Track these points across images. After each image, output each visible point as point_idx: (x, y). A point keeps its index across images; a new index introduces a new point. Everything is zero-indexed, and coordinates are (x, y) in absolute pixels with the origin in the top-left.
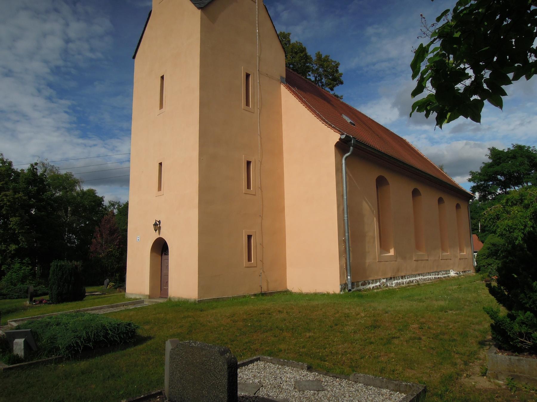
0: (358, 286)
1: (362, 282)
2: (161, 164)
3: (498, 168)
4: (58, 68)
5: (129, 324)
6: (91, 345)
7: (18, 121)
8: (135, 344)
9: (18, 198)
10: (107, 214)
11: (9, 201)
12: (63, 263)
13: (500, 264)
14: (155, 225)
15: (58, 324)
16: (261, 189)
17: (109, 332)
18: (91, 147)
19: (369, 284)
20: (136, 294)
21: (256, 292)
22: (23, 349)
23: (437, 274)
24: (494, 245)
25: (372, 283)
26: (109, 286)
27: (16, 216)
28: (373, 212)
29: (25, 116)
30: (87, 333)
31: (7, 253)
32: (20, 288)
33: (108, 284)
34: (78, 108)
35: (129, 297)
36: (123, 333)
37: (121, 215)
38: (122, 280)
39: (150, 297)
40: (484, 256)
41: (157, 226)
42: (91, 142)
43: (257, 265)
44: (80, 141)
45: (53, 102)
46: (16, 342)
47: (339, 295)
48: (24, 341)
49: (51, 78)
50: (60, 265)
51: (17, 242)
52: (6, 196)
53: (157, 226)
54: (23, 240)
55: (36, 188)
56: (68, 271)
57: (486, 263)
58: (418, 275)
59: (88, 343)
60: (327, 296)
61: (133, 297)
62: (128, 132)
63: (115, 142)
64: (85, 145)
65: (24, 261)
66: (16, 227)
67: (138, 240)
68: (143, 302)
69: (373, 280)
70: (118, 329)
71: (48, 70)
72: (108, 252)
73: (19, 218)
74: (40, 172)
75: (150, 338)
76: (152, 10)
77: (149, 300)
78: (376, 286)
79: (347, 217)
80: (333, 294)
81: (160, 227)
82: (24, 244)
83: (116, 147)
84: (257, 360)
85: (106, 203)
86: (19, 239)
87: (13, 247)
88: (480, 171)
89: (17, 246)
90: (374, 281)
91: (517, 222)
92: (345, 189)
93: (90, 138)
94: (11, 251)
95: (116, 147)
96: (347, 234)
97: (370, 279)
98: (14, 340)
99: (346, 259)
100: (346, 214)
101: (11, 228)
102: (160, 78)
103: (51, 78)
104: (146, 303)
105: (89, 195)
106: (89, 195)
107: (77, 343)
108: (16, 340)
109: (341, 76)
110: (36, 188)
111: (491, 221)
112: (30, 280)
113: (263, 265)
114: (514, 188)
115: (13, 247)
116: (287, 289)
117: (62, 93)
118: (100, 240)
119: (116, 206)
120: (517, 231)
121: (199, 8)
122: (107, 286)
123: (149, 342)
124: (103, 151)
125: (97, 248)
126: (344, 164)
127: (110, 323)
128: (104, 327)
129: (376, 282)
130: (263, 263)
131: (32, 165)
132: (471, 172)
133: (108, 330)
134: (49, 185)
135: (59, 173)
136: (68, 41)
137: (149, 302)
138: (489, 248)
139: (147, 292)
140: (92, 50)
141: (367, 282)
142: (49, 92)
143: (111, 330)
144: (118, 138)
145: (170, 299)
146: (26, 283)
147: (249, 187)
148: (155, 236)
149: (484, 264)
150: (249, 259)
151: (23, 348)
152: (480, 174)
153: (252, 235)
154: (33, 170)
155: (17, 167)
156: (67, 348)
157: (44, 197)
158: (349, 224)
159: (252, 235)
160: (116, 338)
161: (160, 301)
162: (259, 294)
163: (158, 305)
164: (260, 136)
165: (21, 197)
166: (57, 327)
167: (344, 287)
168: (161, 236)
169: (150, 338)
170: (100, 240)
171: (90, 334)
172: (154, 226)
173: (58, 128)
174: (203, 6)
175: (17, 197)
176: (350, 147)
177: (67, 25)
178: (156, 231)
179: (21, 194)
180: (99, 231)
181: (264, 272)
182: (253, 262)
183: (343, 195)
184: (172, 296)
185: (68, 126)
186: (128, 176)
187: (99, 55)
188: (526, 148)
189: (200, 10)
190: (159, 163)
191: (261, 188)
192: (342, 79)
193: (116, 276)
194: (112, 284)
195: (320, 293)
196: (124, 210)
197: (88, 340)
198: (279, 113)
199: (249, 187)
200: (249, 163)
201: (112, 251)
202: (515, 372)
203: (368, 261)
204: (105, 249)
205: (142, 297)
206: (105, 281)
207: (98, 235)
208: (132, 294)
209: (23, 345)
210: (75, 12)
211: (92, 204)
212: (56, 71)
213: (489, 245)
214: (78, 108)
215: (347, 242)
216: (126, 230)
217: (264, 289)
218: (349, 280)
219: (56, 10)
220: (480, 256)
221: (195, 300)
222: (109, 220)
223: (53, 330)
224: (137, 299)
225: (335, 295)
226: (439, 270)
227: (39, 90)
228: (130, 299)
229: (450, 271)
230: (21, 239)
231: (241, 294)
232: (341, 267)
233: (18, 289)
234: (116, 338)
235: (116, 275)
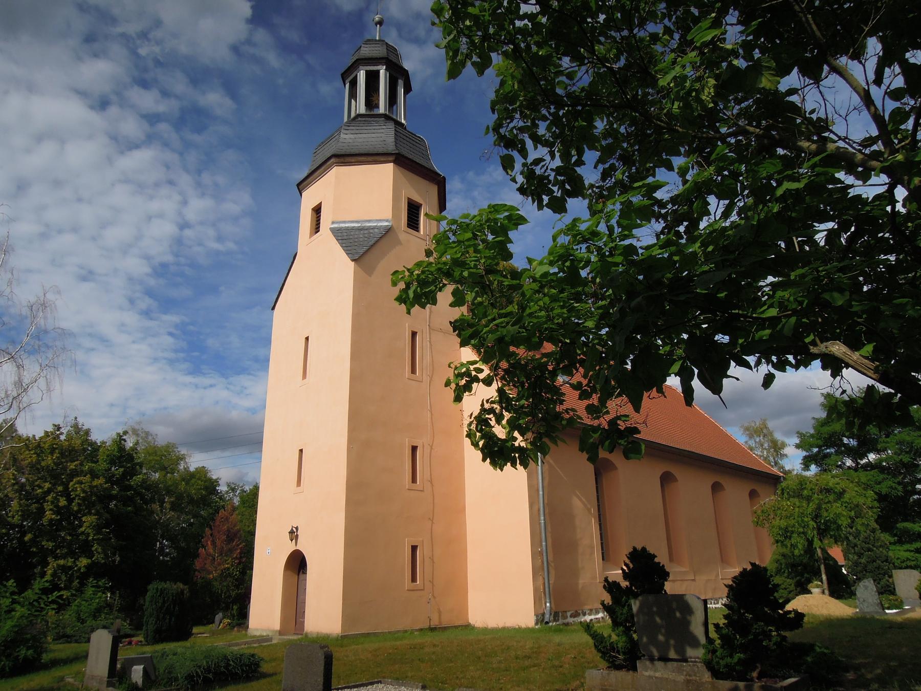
0: (566, 618)
1: (572, 612)
2: (301, 451)
4: (164, 266)
5: (253, 656)
6: (210, 676)
7: (93, 349)
8: (258, 678)
9: (96, 486)
10: (223, 507)
11: (84, 491)
12: (165, 586)
13: (793, 585)
14: (292, 532)
15: (175, 654)
16: (431, 483)
17: (231, 663)
18: (205, 388)
19: (584, 614)
20: (263, 630)
21: (421, 626)
23: (713, 601)
25: (590, 614)
26: (221, 624)
27: (90, 513)
28: (589, 510)
29: (104, 341)
30: (207, 662)
31: (73, 571)
32: (92, 626)
33: (221, 622)
34: (191, 328)
35: (252, 635)
36: (246, 666)
37: (244, 507)
38: (243, 615)
39: (281, 633)
41: (294, 534)
42: (207, 381)
44: (189, 379)
45: (151, 319)
48: (144, 668)
49: (152, 282)
50: (161, 589)
51: (90, 555)
52: (81, 483)
53: (294, 534)
54: (100, 550)
55: (122, 470)
56: (171, 597)
59: (209, 673)
60: (519, 631)
61: (258, 633)
62: (264, 363)
63: (244, 380)
64: (197, 386)
65: (100, 583)
66: (90, 531)
69: (591, 610)
70: (241, 660)
71: (148, 270)
72: (222, 571)
73: (96, 517)
74: (129, 443)
75: (275, 674)
77: (280, 637)
78: (596, 618)
79: (545, 520)
80: (525, 629)
81: (297, 536)
82: (99, 557)
83: (245, 388)
84: (378, 682)
85: (223, 488)
86: (93, 549)
87: (84, 562)
88: (812, 431)
89: (89, 561)
90: (594, 610)
91: (793, 521)
92: (540, 481)
93: (204, 374)
94: (80, 569)
95: (245, 388)
96: (544, 543)
97: (586, 608)
98: (132, 667)
99: (544, 579)
101: (84, 532)
103: (152, 282)
104: (274, 642)
105: (199, 479)
106: (199, 479)
107: (197, 672)
108: (135, 667)
110: (122, 470)
112: (106, 614)
113: (433, 588)
115: (84, 562)
117: (167, 304)
118: (211, 551)
119: (238, 492)
120: (795, 535)
122: (219, 625)
123: (274, 677)
124: (224, 394)
125: (205, 564)
127: (232, 653)
128: (225, 657)
129: (596, 612)
130: (433, 585)
131: (118, 434)
132: (798, 433)
133: (229, 660)
134: (141, 465)
135: (156, 443)
136: (184, 225)
137: (280, 639)
138: (778, 560)
139: (277, 626)
140: (220, 239)
141: (581, 612)
142: (145, 303)
143: (233, 661)
144: (249, 374)
145: (306, 635)
146: (100, 619)
147: (414, 480)
148: (290, 547)
150: (414, 579)
152: (812, 436)
154: (120, 442)
155: (97, 437)
156: (186, 678)
157: (132, 483)
158: (549, 528)
160: (238, 670)
162: (426, 629)
163: (291, 644)
164: (431, 412)
165: (101, 485)
166: (175, 657)
167: (540, 619)
168: (299, 547)
169: (275, 674)
170: (211, 551)
171: (210, 663)
173: (156, 360)
175: (95, 484)
177: (185, 203)
178: (292, 540)
179: (101, 481)
180: (211, 535)
181: (434, 597)
183: (538, 490)
185: (172, 355)
186: (261, 433)
187: (231, 245)
191: (431, 482)
193: (233, 609)
194: (227, 621)
196: (251, 499)
197: (208, 670)
199: (414, 480)
200: (414, 449)
201: (228, 569)
202: (605, 686)
203: (581, 582)
204: (219, 564)
205: (270, 634)
206: (217, 616)
207: (209, 543)
208: (257, 630)
209: (142, 672)
210: (199, 185)
211: (202, 493)
212: (161, 270)
214: (191, 328)
215: (544, 554)
216: (253, 534)
217: (435, 622)
218: (548, 609)
219: (171, 183)
221: (338, 636)
222: (227, 518)
223: (170, 659)
224: (263, 636)
225: (529, 630)
226: (717, 596)
227: (132, 301)
228: (255, 636)
230: (96, 550)
231: (400, 628)
232: (536, 590)
233: (89, 627)
234: (238, 670)
235: (232, 607)
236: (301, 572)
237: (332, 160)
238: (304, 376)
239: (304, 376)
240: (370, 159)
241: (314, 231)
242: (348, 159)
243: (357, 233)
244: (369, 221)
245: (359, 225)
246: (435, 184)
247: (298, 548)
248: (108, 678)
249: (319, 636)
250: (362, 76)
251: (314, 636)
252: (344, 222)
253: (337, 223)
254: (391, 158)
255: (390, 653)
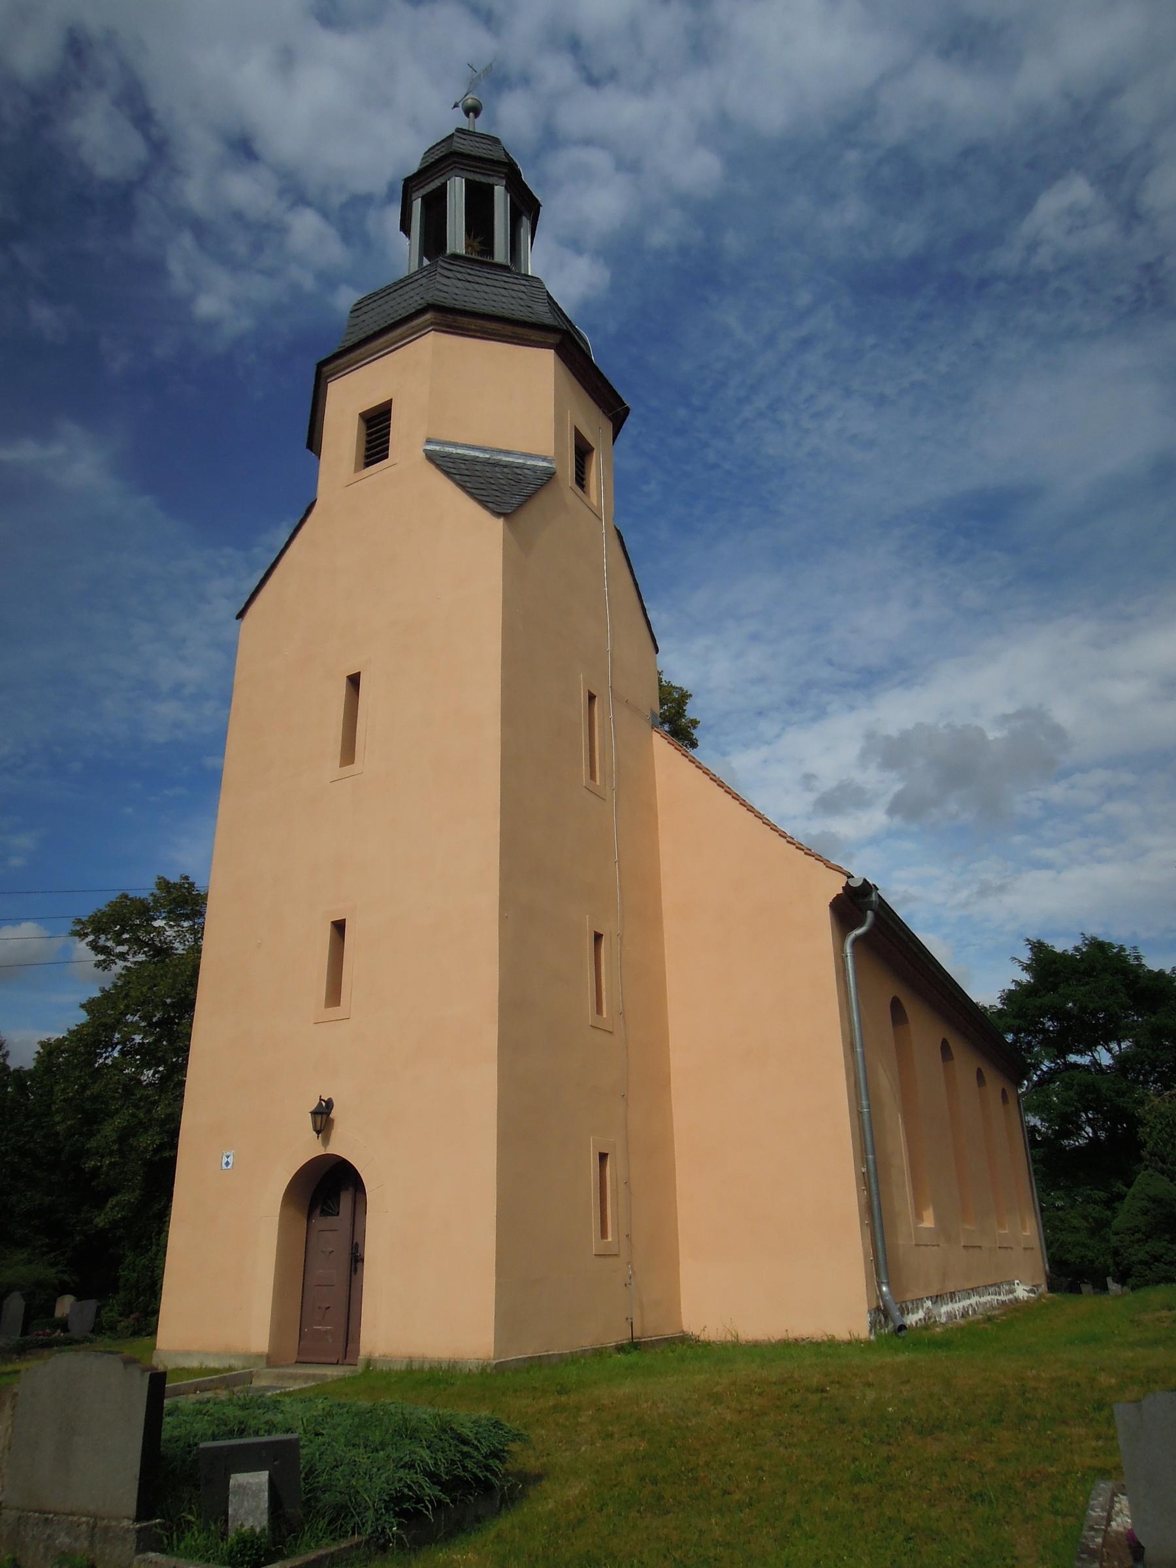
2: (339, 927)
3: (1049, 998)
22: (266, 1511)
24: (1154, 1200)
39: (270, 1360)
40: (1137, 1234)
41: (323, 1116)
43: (619, 1252)
46: (240, 1486)
47: (868, 1343)
53: (323, 1116)
57: (1147, 1252)
58: (970, 1291)
60: (826, 1348)
67: (227, 1163)
68: (250, 1376)
76: (316, 500)
100: (864, 1097)
102: (343, 683)
108: (238, 1479)
109: (695, 728)
111: (1166, 1131)
114: (1092, 1054)
116: (683, 1331)
121: (499, 514)
126: (849, 957)
139: (259, 1340)
148: (308, 1148)
149: (1142, 1255)
151: (267, 1506)
153: (607, 1154)
159: (607, 1154)
161: (335, 1373)
172: (319, 1118)
174: (509, 511)
176: (866, 911)
182: (610, 1239)
184: (377, 1355)
188: (1115, 951)
189: (502, 519)
190: (332, 922)
192: (696, 734)
195: (803, 1340)
198: (651, 808)
213: (1145, 1203)
220: (1122, 1233)
229: (1014, 1284)
236: (318, 1211)
237: (428, 316)
238: (348, 753)
239: (348, 753)
240: (508, 329)
241: (362, 461)
242: (463, 321)
243: (487, 468)
244: (508, 453)
245: (488, 456)
246: (610, 419)
247: (331, 1150)
248: (138, 1519)
249: (415, 1366)
250: (456, 191)
251: (400, 1366)
252: (455, 445)
253: (438, 443)
254: (554, 338)
255: (780, 1415)
